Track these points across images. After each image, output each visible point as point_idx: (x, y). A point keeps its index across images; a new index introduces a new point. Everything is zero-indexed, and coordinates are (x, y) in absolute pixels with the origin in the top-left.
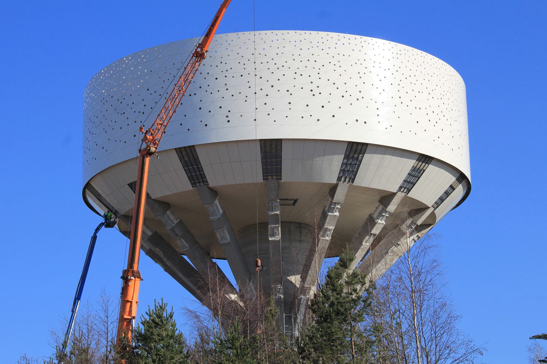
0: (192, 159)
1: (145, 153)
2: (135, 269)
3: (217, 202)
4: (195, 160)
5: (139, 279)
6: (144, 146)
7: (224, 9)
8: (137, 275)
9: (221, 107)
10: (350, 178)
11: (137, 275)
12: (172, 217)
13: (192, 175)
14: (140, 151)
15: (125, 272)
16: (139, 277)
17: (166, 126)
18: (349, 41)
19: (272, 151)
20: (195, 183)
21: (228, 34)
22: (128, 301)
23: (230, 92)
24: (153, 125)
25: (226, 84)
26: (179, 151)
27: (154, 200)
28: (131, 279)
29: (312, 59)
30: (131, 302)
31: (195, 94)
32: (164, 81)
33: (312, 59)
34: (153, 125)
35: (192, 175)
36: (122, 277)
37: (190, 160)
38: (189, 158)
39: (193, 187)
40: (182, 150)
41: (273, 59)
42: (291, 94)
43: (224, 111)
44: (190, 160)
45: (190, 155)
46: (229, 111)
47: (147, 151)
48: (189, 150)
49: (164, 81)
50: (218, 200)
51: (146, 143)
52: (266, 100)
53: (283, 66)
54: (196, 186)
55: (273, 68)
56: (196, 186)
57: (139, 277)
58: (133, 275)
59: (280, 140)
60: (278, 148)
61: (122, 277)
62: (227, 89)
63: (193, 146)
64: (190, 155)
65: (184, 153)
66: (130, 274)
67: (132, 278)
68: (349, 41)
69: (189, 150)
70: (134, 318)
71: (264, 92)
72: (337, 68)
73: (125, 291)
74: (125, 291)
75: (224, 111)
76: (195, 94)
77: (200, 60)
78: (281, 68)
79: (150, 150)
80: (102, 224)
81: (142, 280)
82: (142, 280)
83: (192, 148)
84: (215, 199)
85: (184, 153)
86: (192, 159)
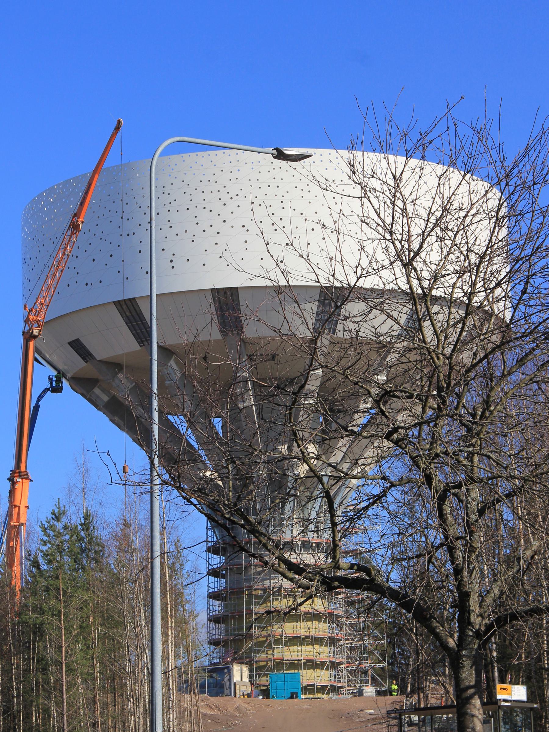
0: (134, 313)
1: (28, 336)
2: (23, 469)
3: (172, 363)
4: (138, 315)
5: (26, 481)
6: (27, 328)
7: (97, 176)
8: (25, 476)
9: (163, 250)
10: (330, 329)
11: (25, 476)
12: (124, 381)
13: (137, 333)
14: (23, 333)
15: (13, 473)
16: (27, 478)
17: (48, 306)
18: (322, 158)
19: (226, 300)
20: (142, 342)
21: (171, 157)
22: (15, 506)
23: (175, 230)
24: (35, 304)
25: (169, 221)
26: (118, 304)
27: (100, 361)
28: (17, 482)
29: (274, 184)
30: (19, 507)
31: (134, 234)
32: (99, 217)
33: (274, 184)
34: (35, 304)
35: (137, 333)
36: (8, 479)
37: (132, 315)
38: (131, 313)
39: (141, 346)
40: (121, 303)
41: (225, 187)
42: (248, 231)
43: (168, 255)
44: (132, 315)
45: (132, 308)
46: (174, 255)
47: (29, 334)
48: (129, 303)
49: (99, 217)
50: (174, 360)
51: (29, 325)
52: (218, 239)
53: (237, 195)
54: (144, 345)
55: (225, 198)
56: (144, 345)
57: (27, 478)
58: (20, 477)
59: (237, 288)
60: (235, 298)
61: (8, 479)
62: (171, 227)
63: (134, 299)
64: (132, 308)
65: (124, 307)
66: (17, 475)
67: (19, 480)
68: (322, 158)
69: (129, 303)
70: (23, 524)
71: (214, 230)
72: (306, 193)
73: (12, 492)
74: (12, 492)
75: (168, 255)
76: (134, 234)
77: (76, 233)
78: (235, 198)
79: (32, 333)
80: (47, 390)
81: (32, 481)
82: (32, 481)
83: (133, 301)
84: (170, 359)
85: (124, 307)
86: (134, 313)
